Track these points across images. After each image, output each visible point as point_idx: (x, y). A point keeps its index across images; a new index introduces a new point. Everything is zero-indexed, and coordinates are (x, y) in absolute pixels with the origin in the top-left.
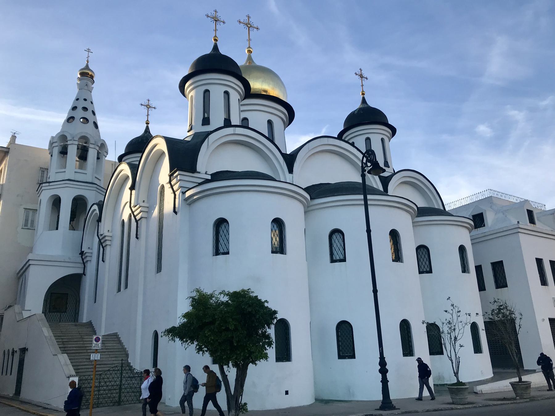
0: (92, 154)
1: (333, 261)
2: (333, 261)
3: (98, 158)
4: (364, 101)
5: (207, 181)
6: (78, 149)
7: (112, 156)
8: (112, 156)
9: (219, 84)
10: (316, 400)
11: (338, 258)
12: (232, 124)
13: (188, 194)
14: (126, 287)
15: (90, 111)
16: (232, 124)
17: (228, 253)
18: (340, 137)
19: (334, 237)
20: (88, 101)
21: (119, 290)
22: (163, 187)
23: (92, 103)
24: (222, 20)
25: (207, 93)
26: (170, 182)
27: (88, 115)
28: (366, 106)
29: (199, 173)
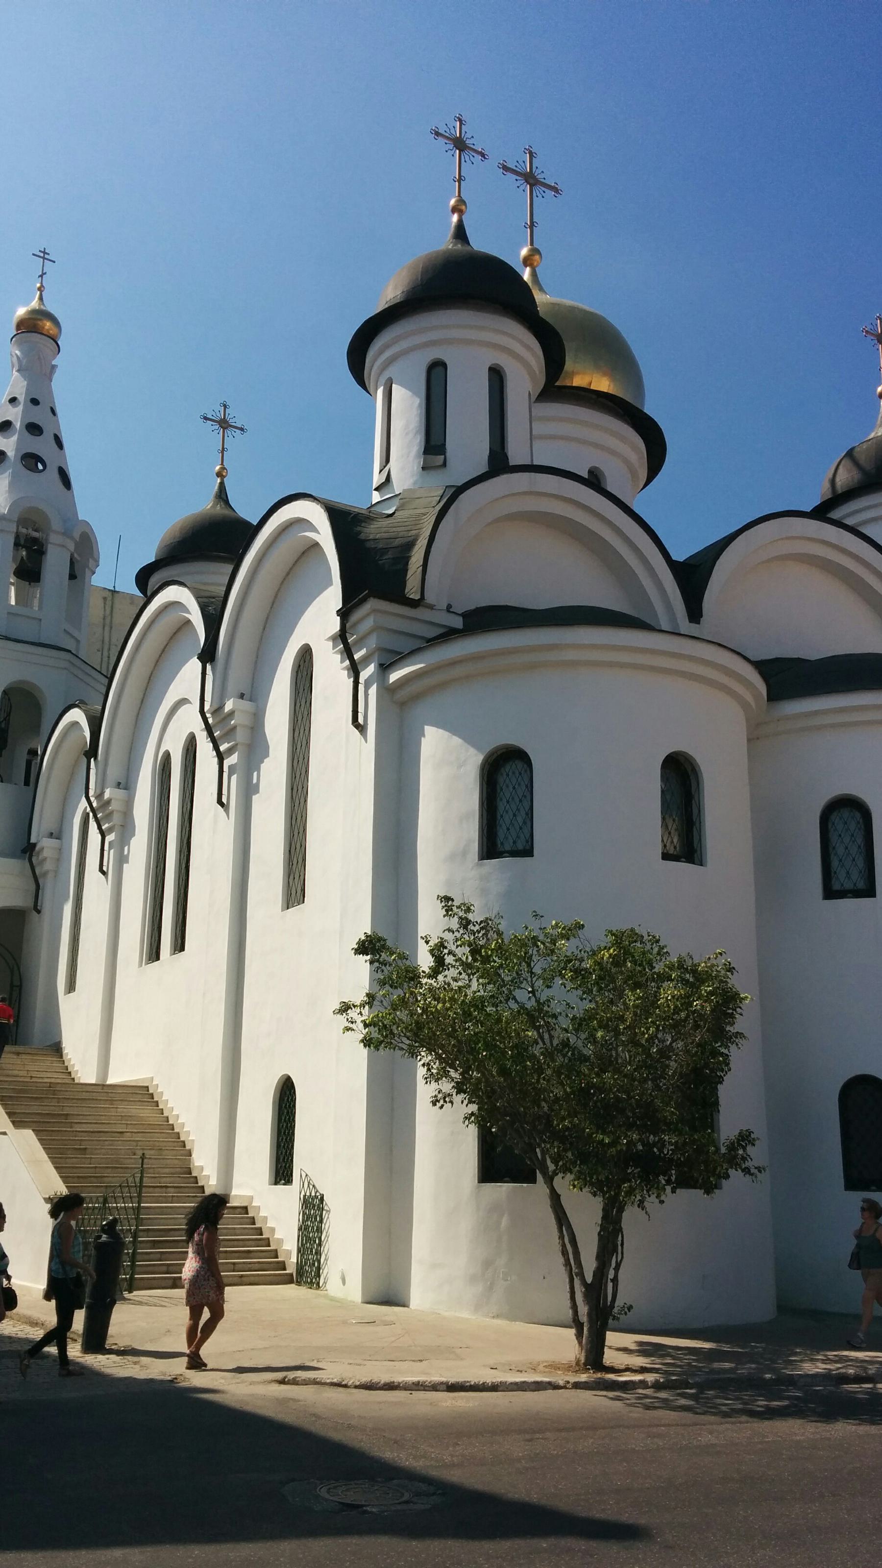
0: (55, 563)
1: (830, 893)
2: (830, 893)
3: (72, 576)
4: (222, 495)
5: (449, 635)
6: (17, 544)
7: (115, 572)
8: (115, 572)
9: (479, 342)
10: (783, 1308)
11: (848, 885)
12: (512, 462)
13: (394, 676)
14: (179, 945)
15: (48, 435)
16: (512, 462)
17: (528, 852)
18: (821, 513)
19: (834, 817)
20: (44, 408)
21: (154, 954)
22: (306, 656)
23: (53, 412)
24: (443, 141)
25: (440, 369)
26: (342, 636)
27: (42, 446)
28: (227, 512)
29: (431, 607)
